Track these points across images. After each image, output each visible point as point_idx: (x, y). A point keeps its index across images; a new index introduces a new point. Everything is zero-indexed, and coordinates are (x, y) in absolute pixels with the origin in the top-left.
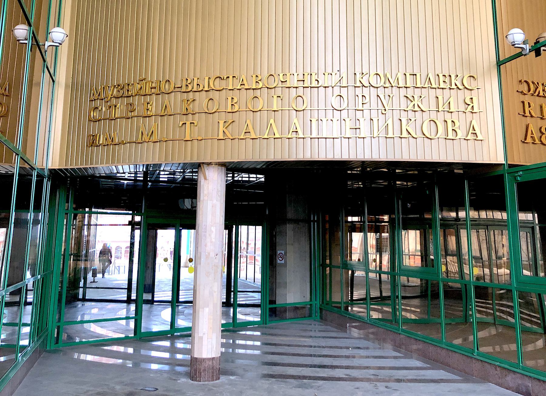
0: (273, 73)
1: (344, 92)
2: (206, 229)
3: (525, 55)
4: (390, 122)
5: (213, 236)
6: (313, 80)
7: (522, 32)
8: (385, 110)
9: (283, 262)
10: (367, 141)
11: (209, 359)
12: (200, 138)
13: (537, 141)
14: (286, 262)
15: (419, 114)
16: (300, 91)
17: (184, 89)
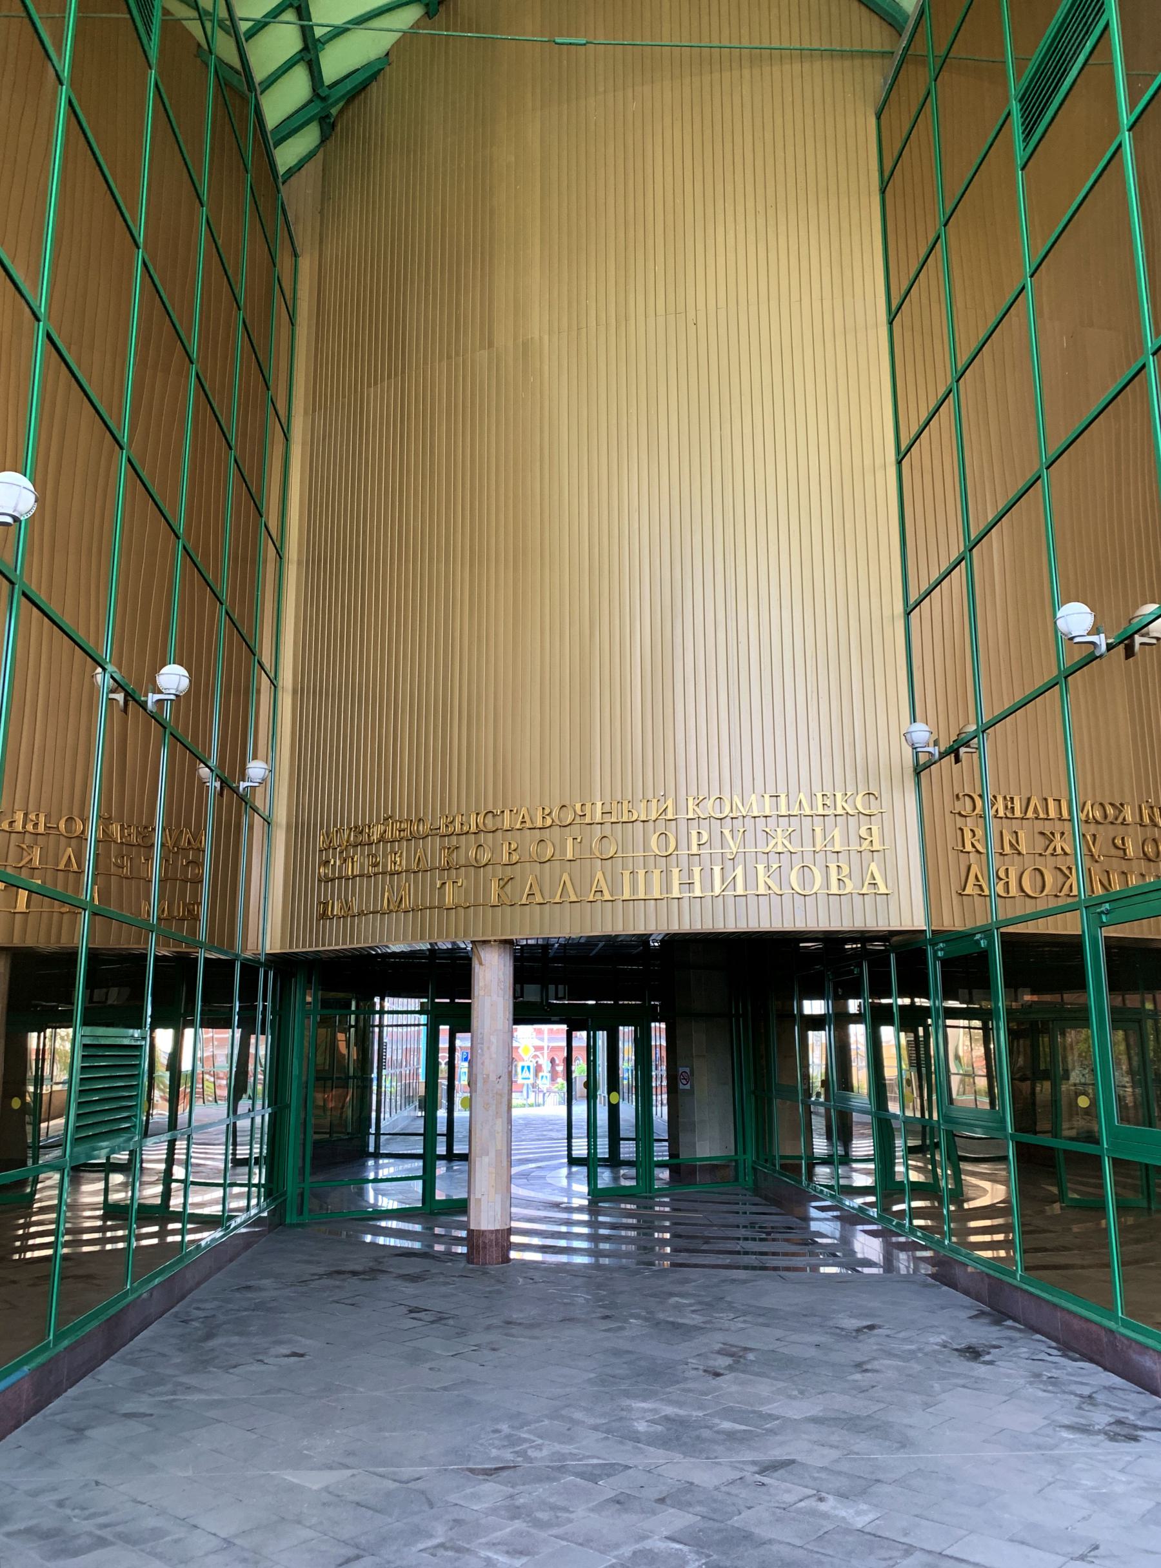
5: (493, 1049)
9: (688, 1087)
11: (491, 1232)
14: (692, 1086)
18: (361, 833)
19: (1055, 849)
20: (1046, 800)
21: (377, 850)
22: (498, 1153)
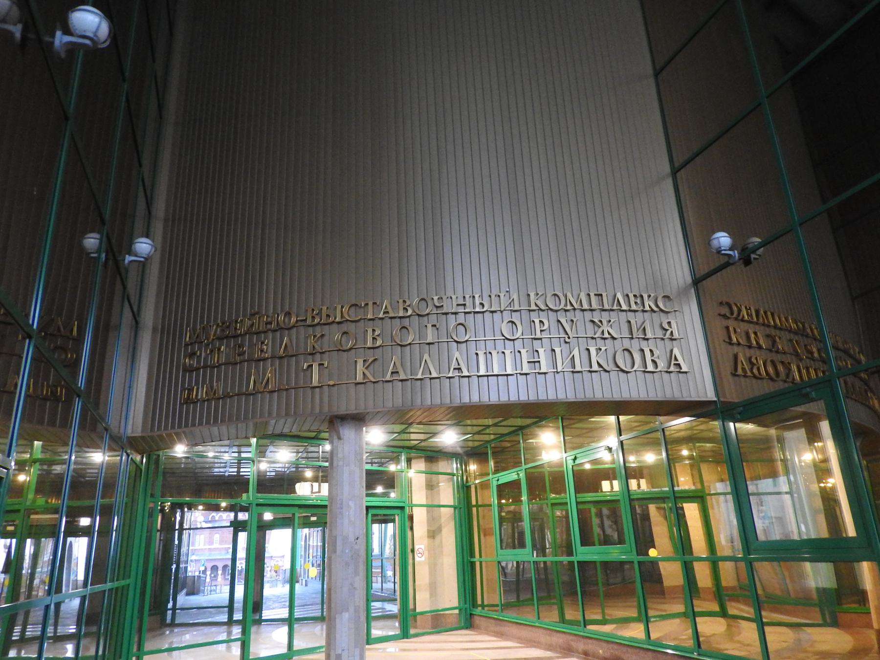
0: (425, 297)
1: (516, 317)
2: (342, 504)
3: (733, 264)
4: (576, 352)
6: (477, 302)
7: (726, 235)
8: (569, 338)
10: (550, 377)
12: (331, 383)
13: (749, 374)
15: (609, 342)
16: (461, 318)
17: (309, 322)
18: (228, 327)
19: (603, 332)
20: (627, 295)
21: (243, 341)
22: (357, 610)
